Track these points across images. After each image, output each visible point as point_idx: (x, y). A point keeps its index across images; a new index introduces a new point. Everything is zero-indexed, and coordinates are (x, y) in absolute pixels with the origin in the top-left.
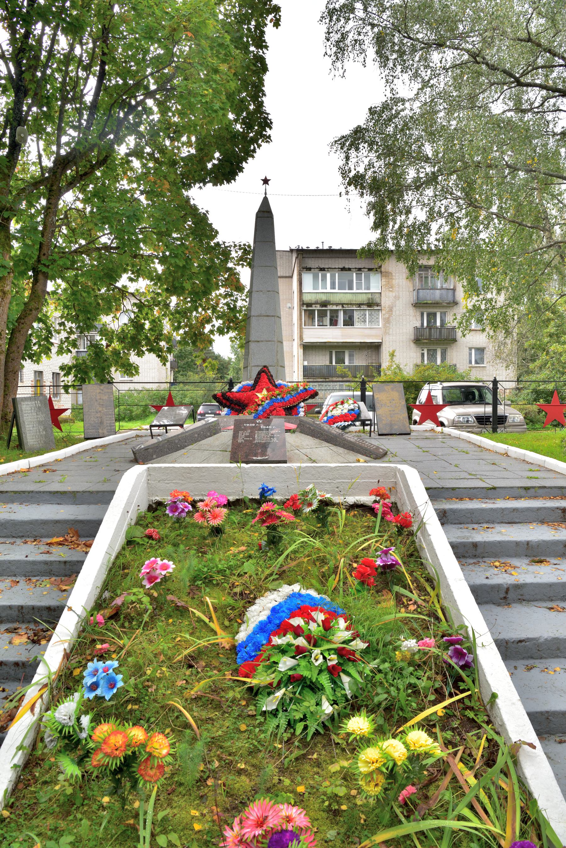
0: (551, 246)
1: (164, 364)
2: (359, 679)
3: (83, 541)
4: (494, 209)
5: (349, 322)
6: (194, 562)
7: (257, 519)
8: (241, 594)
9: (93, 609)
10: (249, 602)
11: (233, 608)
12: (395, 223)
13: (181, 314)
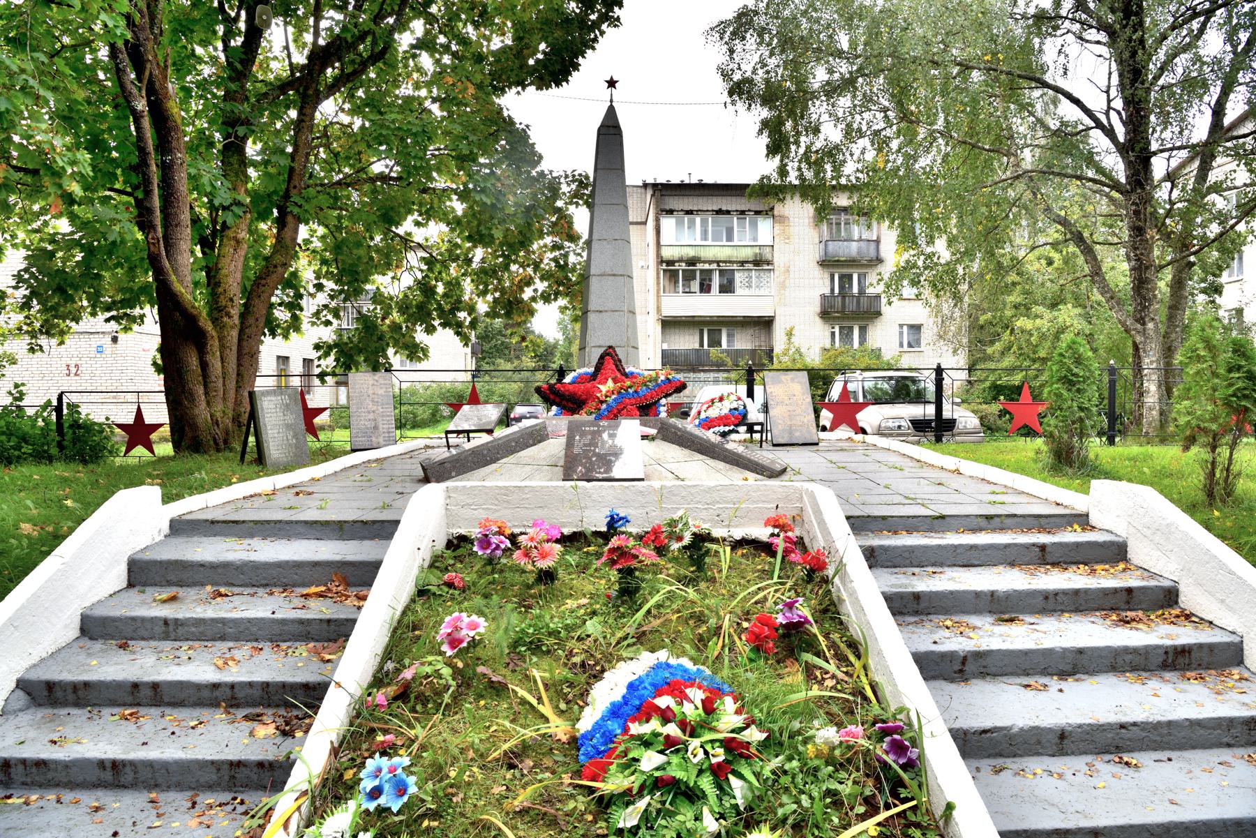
0: (1017, 177)
1: (466, 345)
2: (756, 784)
3: (352, 591)
4: (940, 124)
5: (727, 288)
6: (514, 621)
7: (603, 559)
8: (583, 665)
9: (371, 686)
10: (595, 677)
11: (571, 685)
12: (799, 146)
13: (485, 275)
